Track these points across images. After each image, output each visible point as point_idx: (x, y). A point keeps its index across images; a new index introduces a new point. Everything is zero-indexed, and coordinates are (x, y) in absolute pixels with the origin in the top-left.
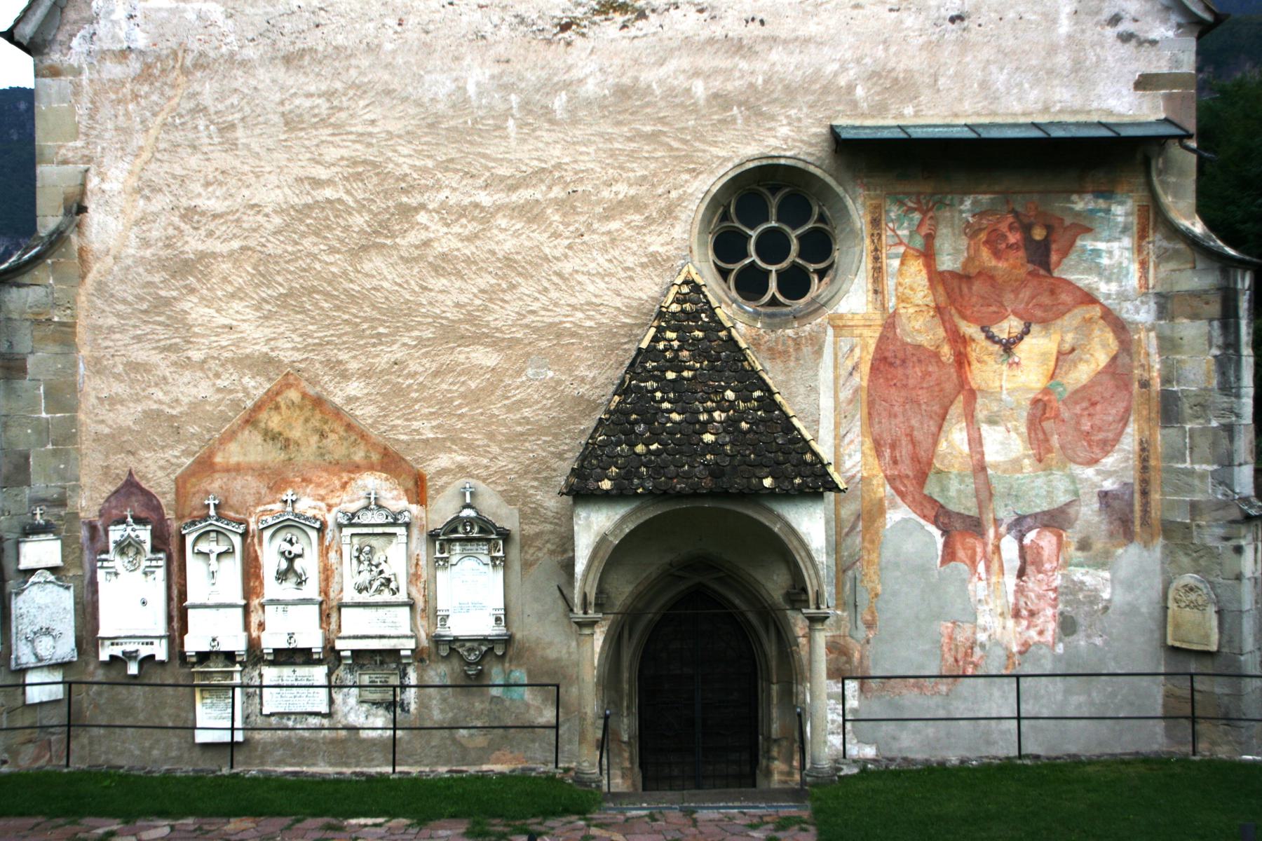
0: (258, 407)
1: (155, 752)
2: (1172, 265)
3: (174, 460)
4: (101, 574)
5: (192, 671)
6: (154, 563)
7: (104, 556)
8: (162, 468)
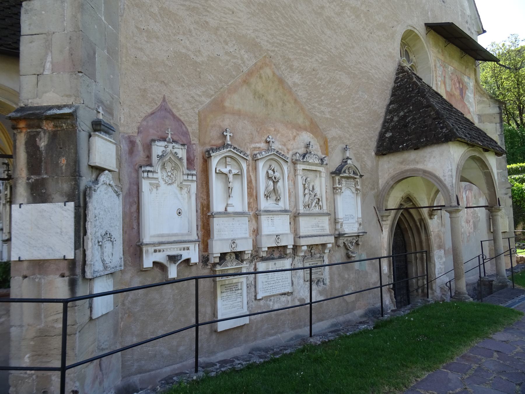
0: (250, 73)
1: (181, 348)
2: (482, 105)
3: (198, 98)
4: (145, 185)
5: (213, 269)
6: (190, 178)
7: (148, 168)
8: (188, 101)
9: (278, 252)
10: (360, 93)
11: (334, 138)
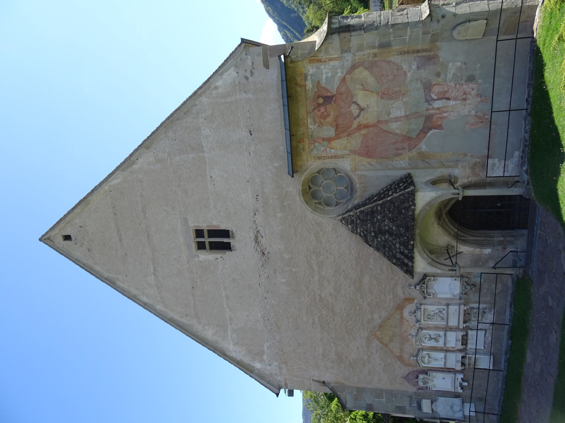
0: (382, 343)
5: (468, 369)
9: (465, 341)
10: (371, 266)
11: (404, 293)
